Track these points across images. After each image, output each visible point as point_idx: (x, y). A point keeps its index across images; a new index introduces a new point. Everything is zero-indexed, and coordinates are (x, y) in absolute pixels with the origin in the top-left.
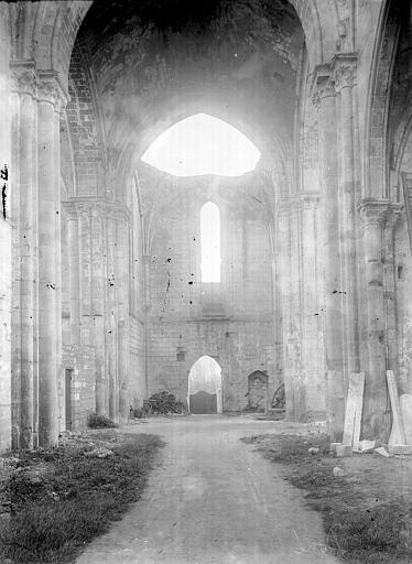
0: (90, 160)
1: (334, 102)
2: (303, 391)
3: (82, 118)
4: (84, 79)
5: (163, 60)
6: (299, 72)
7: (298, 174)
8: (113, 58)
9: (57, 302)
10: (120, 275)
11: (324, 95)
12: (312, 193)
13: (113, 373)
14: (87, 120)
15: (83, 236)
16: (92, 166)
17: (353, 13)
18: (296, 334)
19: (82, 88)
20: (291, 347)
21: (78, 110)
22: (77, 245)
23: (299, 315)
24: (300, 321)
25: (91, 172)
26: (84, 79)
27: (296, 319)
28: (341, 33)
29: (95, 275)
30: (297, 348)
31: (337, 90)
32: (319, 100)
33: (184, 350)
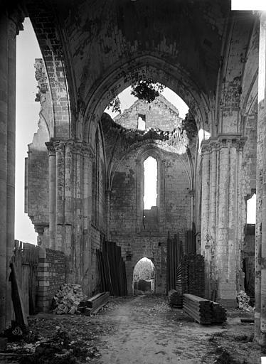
2: (217, 283)
3: (58, 75)
4: (58, 39)
5: (120, 31)
6: (224, 36)
7: (218, 120)
8: (82, 25)
9: (64, 238)
10: (86, 228)
12: (228, 135)
13: (78, 266)
15: (59, 166)
18: (211, 242)
19: (57, 47)
21: (54, 68)
22: (55, 174)
24: (215, 233)
26: (58, 39)
27: (212, 230)
30: (212, 253)
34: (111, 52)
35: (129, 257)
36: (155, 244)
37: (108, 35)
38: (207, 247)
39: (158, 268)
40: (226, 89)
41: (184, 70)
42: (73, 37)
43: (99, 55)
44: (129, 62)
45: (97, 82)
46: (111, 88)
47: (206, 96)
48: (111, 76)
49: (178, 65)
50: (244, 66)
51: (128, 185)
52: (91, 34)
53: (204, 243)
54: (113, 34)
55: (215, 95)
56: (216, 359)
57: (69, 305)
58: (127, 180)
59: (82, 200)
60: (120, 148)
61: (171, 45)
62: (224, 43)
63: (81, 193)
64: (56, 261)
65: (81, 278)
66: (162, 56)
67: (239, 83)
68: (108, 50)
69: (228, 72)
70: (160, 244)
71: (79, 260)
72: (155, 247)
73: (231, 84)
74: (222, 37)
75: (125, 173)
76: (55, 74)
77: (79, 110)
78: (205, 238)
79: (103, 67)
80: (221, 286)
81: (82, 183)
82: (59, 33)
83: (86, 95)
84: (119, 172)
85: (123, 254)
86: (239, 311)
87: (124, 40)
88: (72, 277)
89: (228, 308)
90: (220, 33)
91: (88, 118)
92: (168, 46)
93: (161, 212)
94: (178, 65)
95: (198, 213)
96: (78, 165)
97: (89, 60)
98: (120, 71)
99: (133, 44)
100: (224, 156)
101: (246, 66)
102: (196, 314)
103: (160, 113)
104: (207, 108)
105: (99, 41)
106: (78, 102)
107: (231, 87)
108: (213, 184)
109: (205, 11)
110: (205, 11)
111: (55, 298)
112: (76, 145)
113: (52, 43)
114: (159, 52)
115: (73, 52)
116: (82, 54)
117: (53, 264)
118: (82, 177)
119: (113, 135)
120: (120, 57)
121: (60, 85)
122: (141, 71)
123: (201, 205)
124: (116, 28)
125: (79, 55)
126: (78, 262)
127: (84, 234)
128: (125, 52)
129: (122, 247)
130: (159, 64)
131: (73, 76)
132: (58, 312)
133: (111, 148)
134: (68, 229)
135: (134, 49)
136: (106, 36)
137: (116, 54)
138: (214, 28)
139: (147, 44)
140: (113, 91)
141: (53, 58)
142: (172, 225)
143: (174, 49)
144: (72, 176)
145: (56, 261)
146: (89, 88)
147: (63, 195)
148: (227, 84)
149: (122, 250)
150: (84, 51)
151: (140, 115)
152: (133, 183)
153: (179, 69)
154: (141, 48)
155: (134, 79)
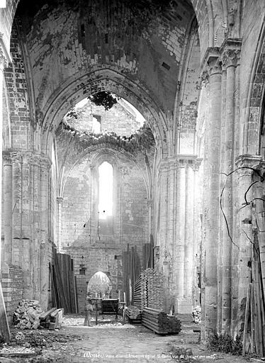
0: (22, 119)
1: (220, 80)
4: (20, 53)
5: (81, 44)
8: (42, 39)
11: (213, 72)
13: (35, 281)
14: (21, 87)
16: (24, 124)
17: (241, 5)
19: (19, 60)
20: (165, 267)
21: (14, 79)
23: (172, 245)
25: (23, 129)
26: (20, 53)
27: (170, 247)
28: (230, 22)
29: (23, 208)
30: (170, 269)
31: (223, 69)
32: (207, 77)
33: (85, 267)
34: (70, 63)
35: (83, 270)
36: (112, 256)
37: (68, 48)
38: (165, 263)
39: (113, 282)
40: (183, 113)
41: (144, 88)
42: (66, 101)
43: (58, 66)
44: (88, 75)
45: (56, 92)
46: (70, 98)
47: (164, 115)
48: (69, 87)
49: (138, 82)
50: (199, 93)
51: (82, 192)
52: (51, 47)
53: (162, 259)
54: (73, 47)
55: (173, 115)
56: (142, 12)
57: (32, 320)
58: (80, 186)
59: (40, 213)
60: (73, 152)
61: (131, 62)
62: (181, 69)
63: (39, 206)
64: (16, 277)
65: (38, 294)
66: (122, 71)
67: (195, 108)
68: (67, 61)
69: (185, 97)
70: (116, 257)
71: (37, 274)
72: (111, 260)
73: (188, 108)
74: (179, 63)
75: (78, 179)
76: (15, 85)
77: (37, 120)
78: (163, 254)
79: (62, 78)
80: (179, 301)
81: (40, 196)
82: (21, 48)
83: (44, 105)
84: (71, 178)
85: (76, 267)
86: (194, 325)
87: (84, 53)
88: (29, 292)
89: (186, 322)
90: (178, 59)
91: (46, 128)
92: (129, 63)
93: (119, 222)
94: (138, 82)
95: (156, 225)
96: (36, 177)
97: (49, 70)
98: (79, 83)
99: (93, 57)
100: (183, 171)
101: (201, 94)
102: (155, 326)
103: (117, 115)
104: (165, 127)
105: (59, 53)
106: (36, 112)
107: (188, 111)
108: (171, 202)
109: (163, 38)
110: (163, 38)
111: (16, 314)
112: (33, 156)
113: (13, 56)
114: (119, 67)
115: (33, 63)
116: (41, 65)
117: (14, 279)
118: (40, 186)
119: (65, 137)
120: (80, 69)
121: (18, 96)
122: (100, 84)
123: (159, 218)
124: (77, 41)
125: (39, 67)
126: (36, 277)
127: (41, 248)
128: (85, 65)
129: (75, 259)
130: (119, 79)
131: (32, 87)
132: (22, 327)
133: (63, 151)
134: (26, 243)
135: (93, 62)
136: (66, 48)
137: (76, 66)
138: (172, 54)
139: (107, 58)
140: (71, 101)
141: (14, 70)
142: (129, 237)
143: (134, 67)
144: (30, 188)
145: (16, 277)
146: (48, 97)
147: (20, 208)
148: (184, 108)
149: (75, 263)
150: (44, 62)
151: (94, 116)
152: (87, 190)
153: (138, 86)
154: (101, 61)
155: (93, 91)
